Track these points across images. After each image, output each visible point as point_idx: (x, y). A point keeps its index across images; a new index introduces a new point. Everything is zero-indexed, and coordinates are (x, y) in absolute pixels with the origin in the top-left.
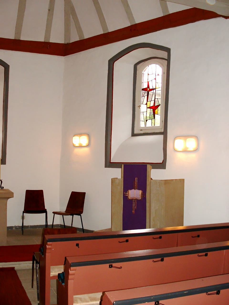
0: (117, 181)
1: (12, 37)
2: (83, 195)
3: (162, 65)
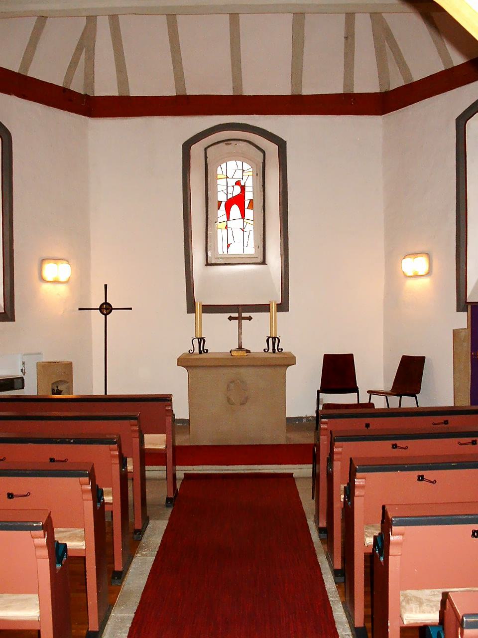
0: (463, 334)
1: (287, 92)
2: (421, 360)
3: (244, 158)
